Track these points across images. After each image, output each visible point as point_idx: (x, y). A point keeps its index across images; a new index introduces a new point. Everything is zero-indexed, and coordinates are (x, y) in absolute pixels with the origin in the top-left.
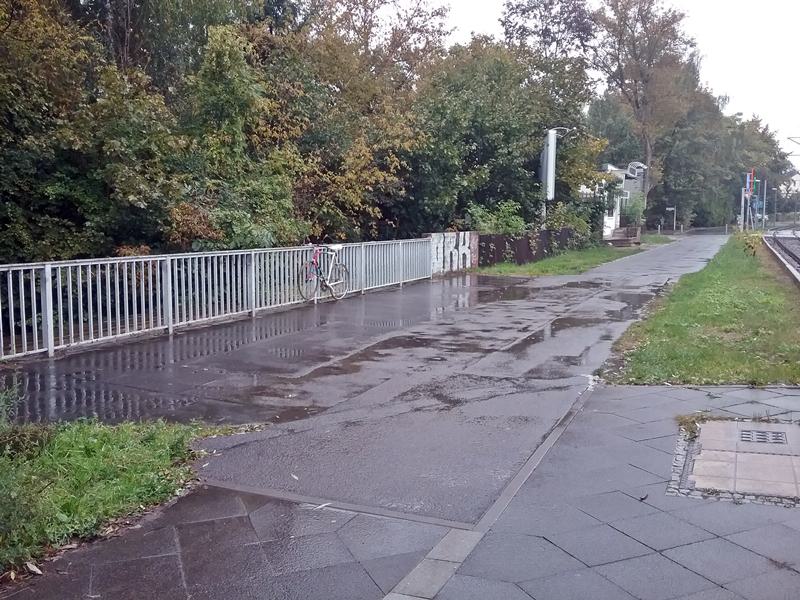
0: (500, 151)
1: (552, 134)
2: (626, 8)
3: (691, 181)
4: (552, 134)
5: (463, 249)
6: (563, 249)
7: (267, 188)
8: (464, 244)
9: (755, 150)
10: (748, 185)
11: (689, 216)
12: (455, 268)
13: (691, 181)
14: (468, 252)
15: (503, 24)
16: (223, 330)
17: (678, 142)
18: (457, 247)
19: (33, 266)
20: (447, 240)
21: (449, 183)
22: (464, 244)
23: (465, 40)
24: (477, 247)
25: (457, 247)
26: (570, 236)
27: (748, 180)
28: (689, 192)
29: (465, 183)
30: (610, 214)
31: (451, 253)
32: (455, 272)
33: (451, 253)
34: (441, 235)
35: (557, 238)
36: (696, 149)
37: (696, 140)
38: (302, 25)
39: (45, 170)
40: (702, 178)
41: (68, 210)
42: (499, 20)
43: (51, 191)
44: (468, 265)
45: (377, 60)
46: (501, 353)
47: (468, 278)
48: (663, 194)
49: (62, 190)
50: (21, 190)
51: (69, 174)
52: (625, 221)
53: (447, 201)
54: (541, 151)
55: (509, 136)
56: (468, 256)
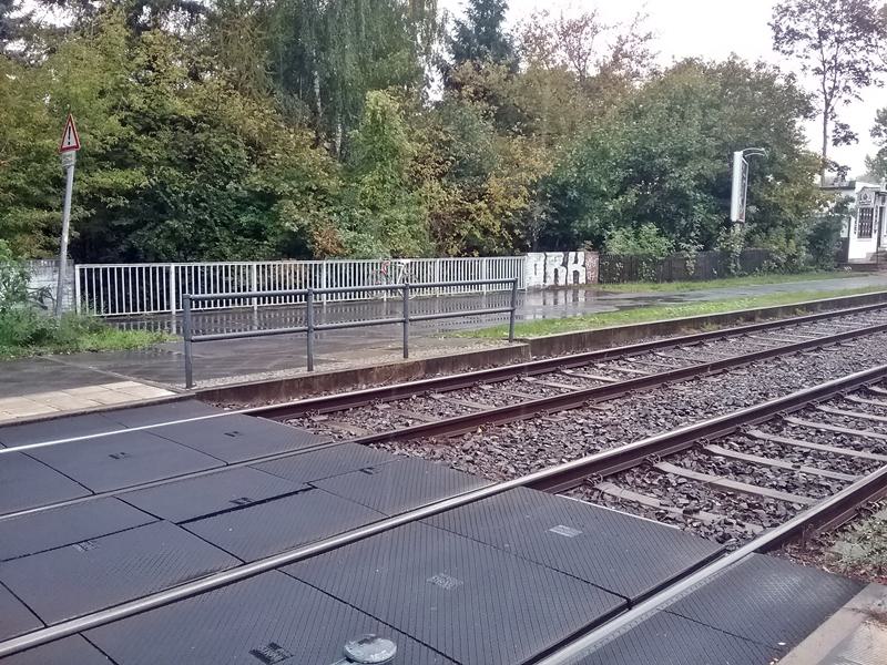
0: (672, 175)
1: (738, 155)
4: (738, 155)
7: (402, 216)
15: (774, 28)
16: (409, 345)
19: (164, 265)
23: (665, 63)
31: (556, 271)
33: (556, 271)
34: (543, 254)
38: (200, 207)
39: (242, 205)
41: (257, 233)
42: (769, 24)
43: (243, 220)
45: (589, 87)
47: (581, 293)
49: (253, 219)
50: (229, 219)
51: (259, 207)
54: (729, 175)
55: (683, 158)
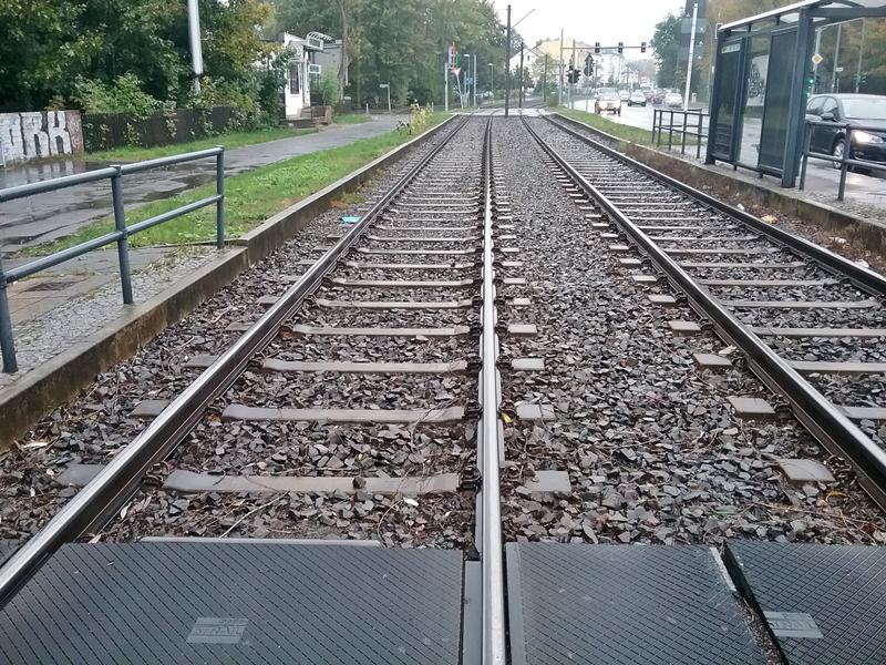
2: (30, 5)
3: (401, 54)
5: (54, 132)
6: (221, 130)
8: (57, 125)
9: (471, 22)
10: (450, 60)
11: (405, 93)
12: (45, 153)
13: (401, 54)
14: (65, 136)
17: (385, 10)
18: (45, 128)
20: (27, 122)
21: (54, 54)
22: (57, 125)
24: (79, 129)
25: (45, 128)
26: (233, 115)
27: (450, 55)
28: (400, 67)
29: (71, 53)
30: (295, 90)
31: (36, 137)
32: (45, 159)
33: (36, 137)
34: (17, 115)
35: (209, 118)
36: (406, 19)
37: (404, 9)
40: (412, 51)
44: (67, 149)
46: (753, 636)
48: (374, 69)
52: (318, 98)
53: (49, 74)
56: (66, 140)
